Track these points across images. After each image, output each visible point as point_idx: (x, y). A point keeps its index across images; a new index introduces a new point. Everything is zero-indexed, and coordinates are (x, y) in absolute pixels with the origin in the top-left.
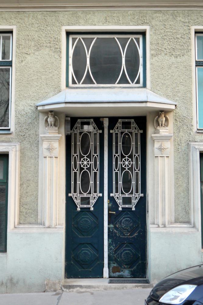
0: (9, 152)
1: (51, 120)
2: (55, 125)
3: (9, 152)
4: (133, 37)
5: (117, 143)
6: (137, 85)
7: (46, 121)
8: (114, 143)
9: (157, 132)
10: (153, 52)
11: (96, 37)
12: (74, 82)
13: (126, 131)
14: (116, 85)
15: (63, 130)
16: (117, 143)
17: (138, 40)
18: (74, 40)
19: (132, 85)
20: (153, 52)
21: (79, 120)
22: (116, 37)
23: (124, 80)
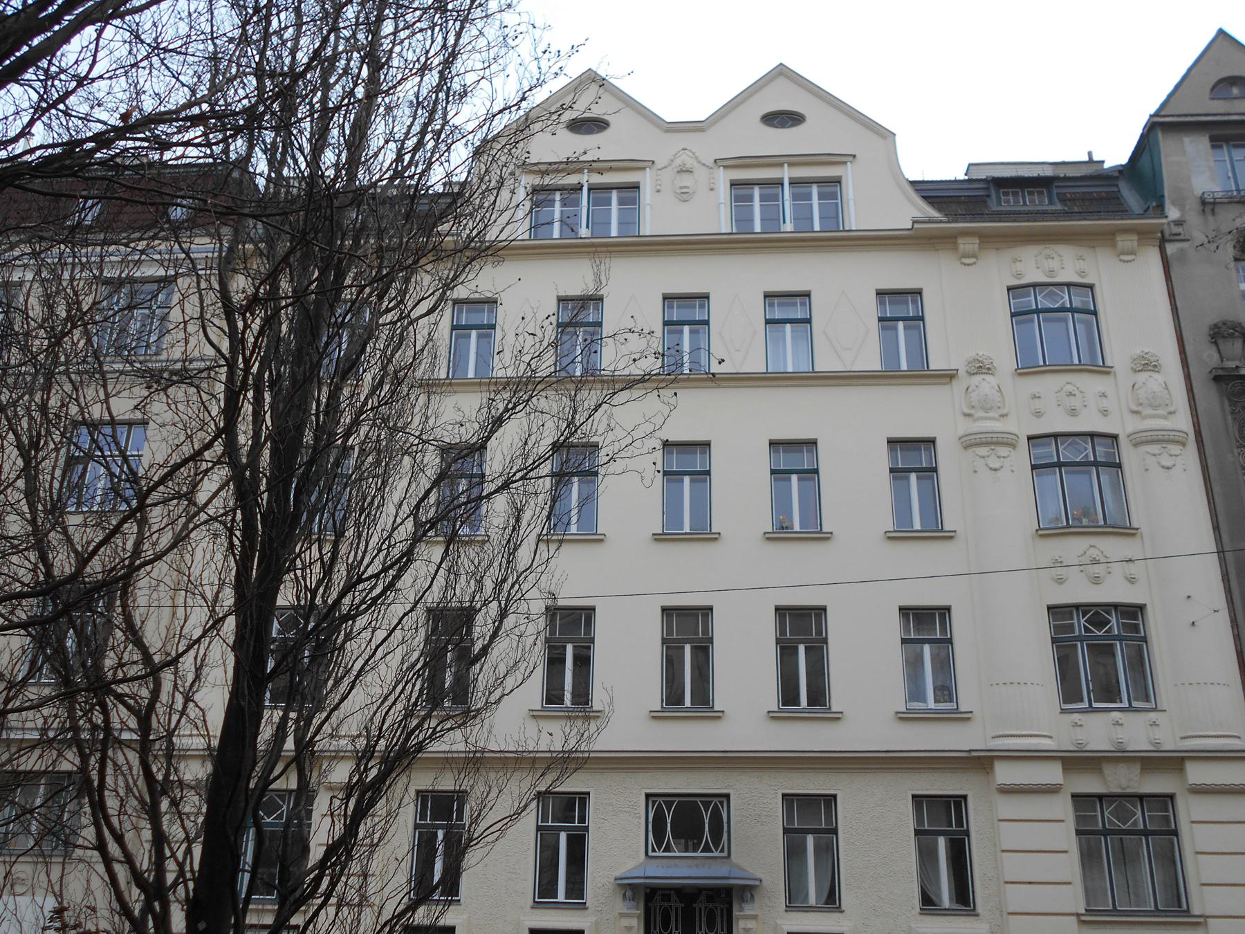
0: (707, 611)
1: (629, 893)
2: (633, 900)
3: (707, 611)
4: (716, 800)
5: (700, 923)
6: (722, 855)
7: (624, 895)
8: (652, 919)
9: (741, 909)
10: (691, 848)
11: (677, 800)
12: (654, 850)
13: (711, 905)
14: (698, 854)
15: (642, 905)
16: (700, 923)
17: (722, 803)
18: (654, 803)
19: (716, 854)
20: (691, 848)
21: (659, 892)
22: (698, 800)
23: (707, 849)
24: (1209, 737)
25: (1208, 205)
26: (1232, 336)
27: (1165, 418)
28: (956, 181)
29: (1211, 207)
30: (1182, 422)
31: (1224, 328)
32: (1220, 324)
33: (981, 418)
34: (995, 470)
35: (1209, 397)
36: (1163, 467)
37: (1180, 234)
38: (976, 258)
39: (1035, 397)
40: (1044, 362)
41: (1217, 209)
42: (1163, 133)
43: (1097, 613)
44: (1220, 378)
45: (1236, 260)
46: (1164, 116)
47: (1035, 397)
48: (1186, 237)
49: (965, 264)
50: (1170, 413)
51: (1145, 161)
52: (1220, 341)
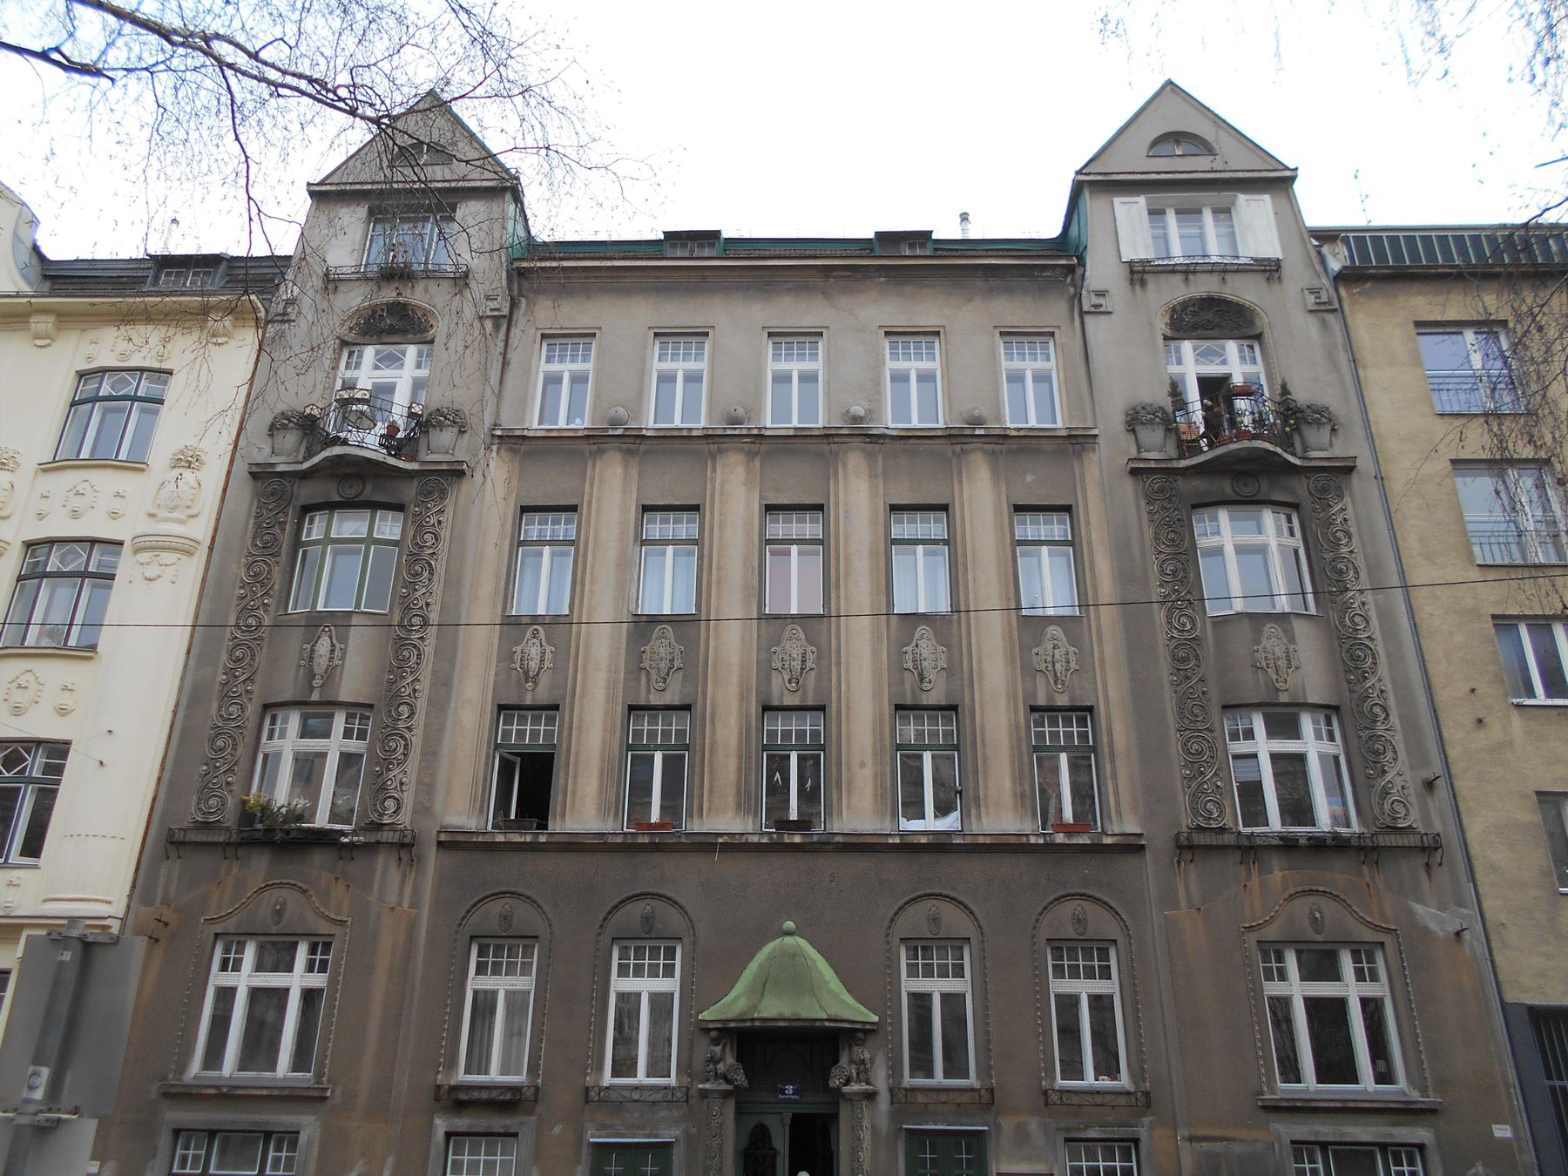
24: (67, 900)
25: (1139, 273)
26: (1151, 422)
27: (181, 522)
28: (131, 260)
29: (1140, 276)
30: (201, 529)
31: (1143, 413)
32: (1139, 408)
33: (166, 520)
34: (150, 580)
35: (243, 493)
36: (150, 580)
37: (1101, 306)
38: (53, 340)
39: (118, 495)
40: (117, 456)
41: (1149, 278)
42: (1091, 193)
43: (16, 751)
44: (260, 474)
45: (1166, 338)
46: (1089, 174)
47: (118, 495)
48: (1109, 310)
49: (38, 346)
50: (192, 516)
51: (1074, 231)
52: (1139, 428)
